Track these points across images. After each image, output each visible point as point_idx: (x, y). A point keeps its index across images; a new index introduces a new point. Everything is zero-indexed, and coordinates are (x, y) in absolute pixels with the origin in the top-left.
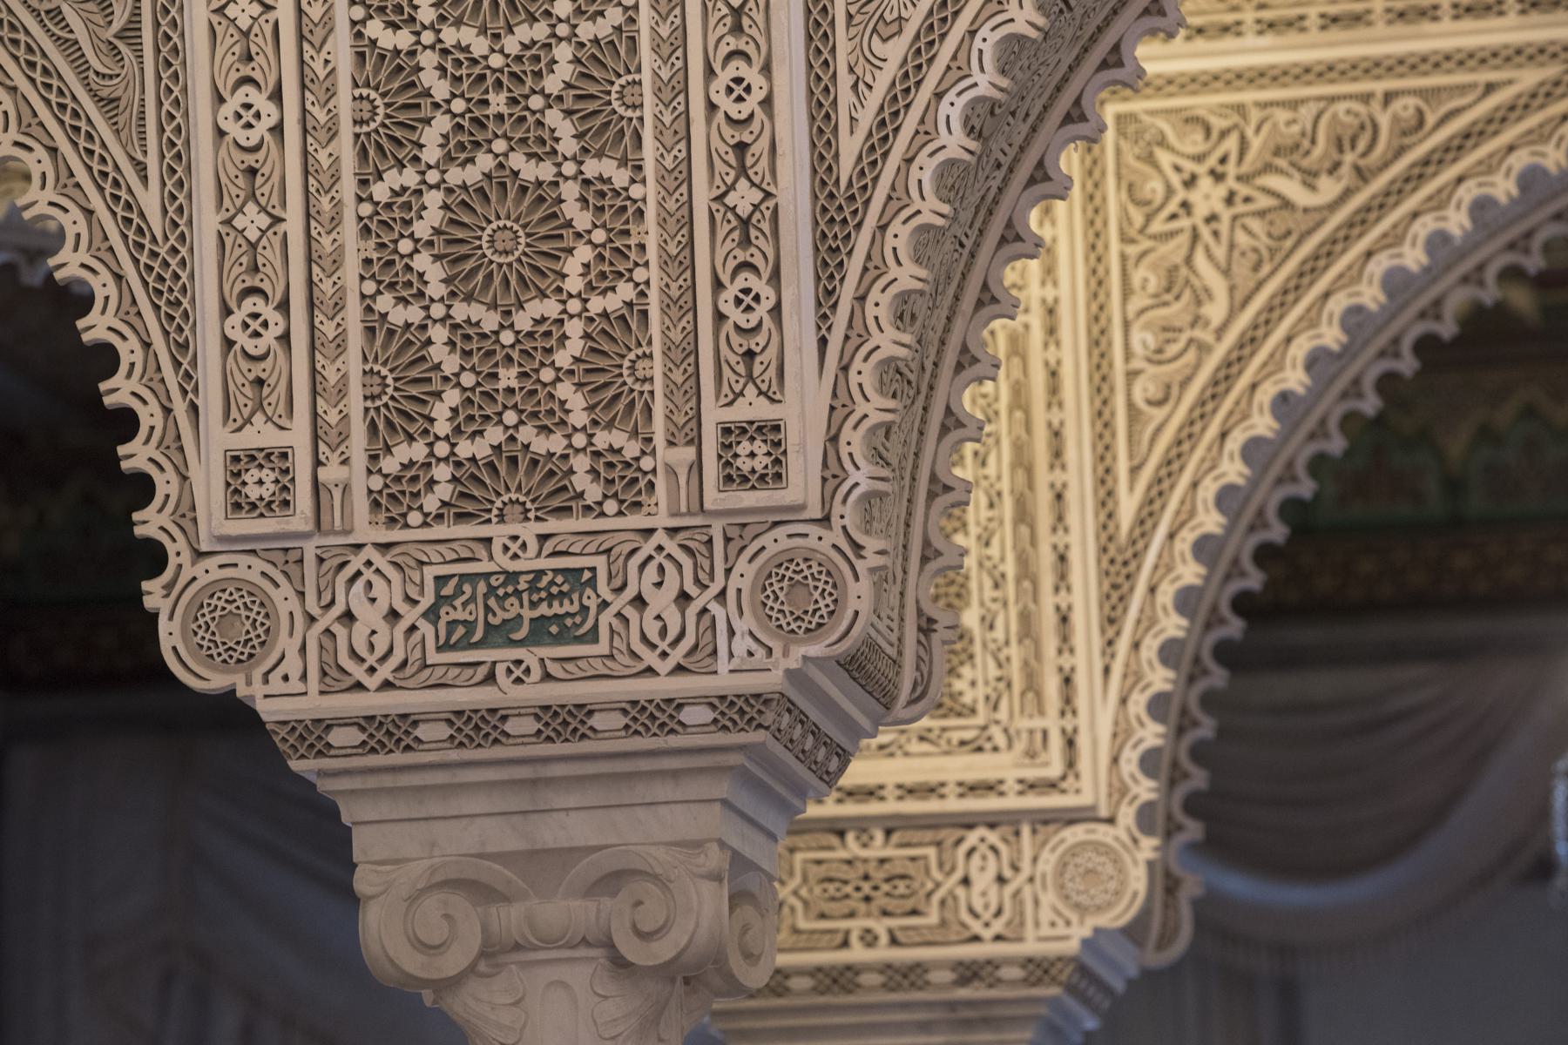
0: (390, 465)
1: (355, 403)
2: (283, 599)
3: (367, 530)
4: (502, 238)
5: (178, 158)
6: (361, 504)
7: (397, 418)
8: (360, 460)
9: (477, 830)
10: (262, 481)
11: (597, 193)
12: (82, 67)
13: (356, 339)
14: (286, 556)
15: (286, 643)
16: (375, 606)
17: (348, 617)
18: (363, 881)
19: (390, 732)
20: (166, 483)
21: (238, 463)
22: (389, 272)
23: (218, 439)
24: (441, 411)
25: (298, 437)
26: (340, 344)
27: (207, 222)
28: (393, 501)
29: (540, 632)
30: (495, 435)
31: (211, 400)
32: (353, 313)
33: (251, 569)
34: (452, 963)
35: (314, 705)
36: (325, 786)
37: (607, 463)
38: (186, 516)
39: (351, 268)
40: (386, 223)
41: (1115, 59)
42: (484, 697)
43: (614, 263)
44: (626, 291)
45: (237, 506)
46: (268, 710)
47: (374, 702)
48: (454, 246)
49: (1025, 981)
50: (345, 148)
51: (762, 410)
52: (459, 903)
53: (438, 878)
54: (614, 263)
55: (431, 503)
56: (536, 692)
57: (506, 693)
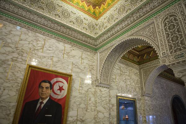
0: (171, 51)
1: (168, 49)
2: (166, 59)
3: (170, 54)
4: (175, 39)
5: (158, 41)
6: (169, 53)
7: (171, 48)
8: (169, 51)
9: (180, 69)
10: (164, 54)
11: (179, 35)
12: (153, 39)
13: (168, 46)
14: (166, 57)
15: (167, 61)
16: (171, 58)
17: (170, 59)
18: (174, 73)
19: (173, 64)
20: (159, 55)
21: (162, 53)
22: (169, 42)
23: (161, 52)
24: (173, 48)
25: (165, 51)
26: (167, 46)
27: (159, 43)
28: (171, 53)
29: (181, 57)
30: (176, 48)
31: (161, 51)
32: (167, 45)
33: (164, 58)
34: (180, 76)
35: (169, 64)
36: (171, 68)
37: (183, 47)
38: (161, 56)
39: (167, 43)
40: (168, 40)
41: (156, 53)
42: (178, 61)
43: (181, 37)
44: (182, 39)
45: (163, 55)
46: (166, 65)
47: (172, 63)
48: (172, 40)
49: (177, 64)
50: (166, 38)
51: (164, 52)
52: (180, 73)
53: (180, 71)
54: (181, 37)
55: (173, 52)
56: (181, 60)
57: (180, 61)
